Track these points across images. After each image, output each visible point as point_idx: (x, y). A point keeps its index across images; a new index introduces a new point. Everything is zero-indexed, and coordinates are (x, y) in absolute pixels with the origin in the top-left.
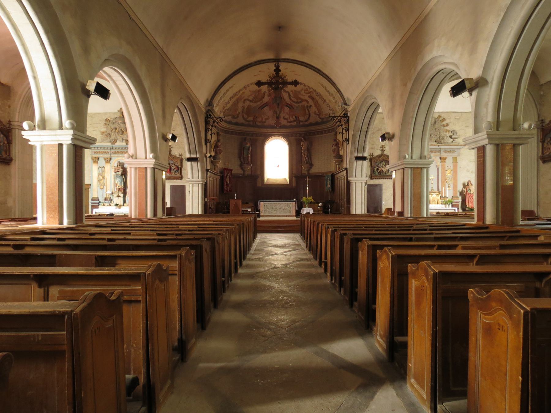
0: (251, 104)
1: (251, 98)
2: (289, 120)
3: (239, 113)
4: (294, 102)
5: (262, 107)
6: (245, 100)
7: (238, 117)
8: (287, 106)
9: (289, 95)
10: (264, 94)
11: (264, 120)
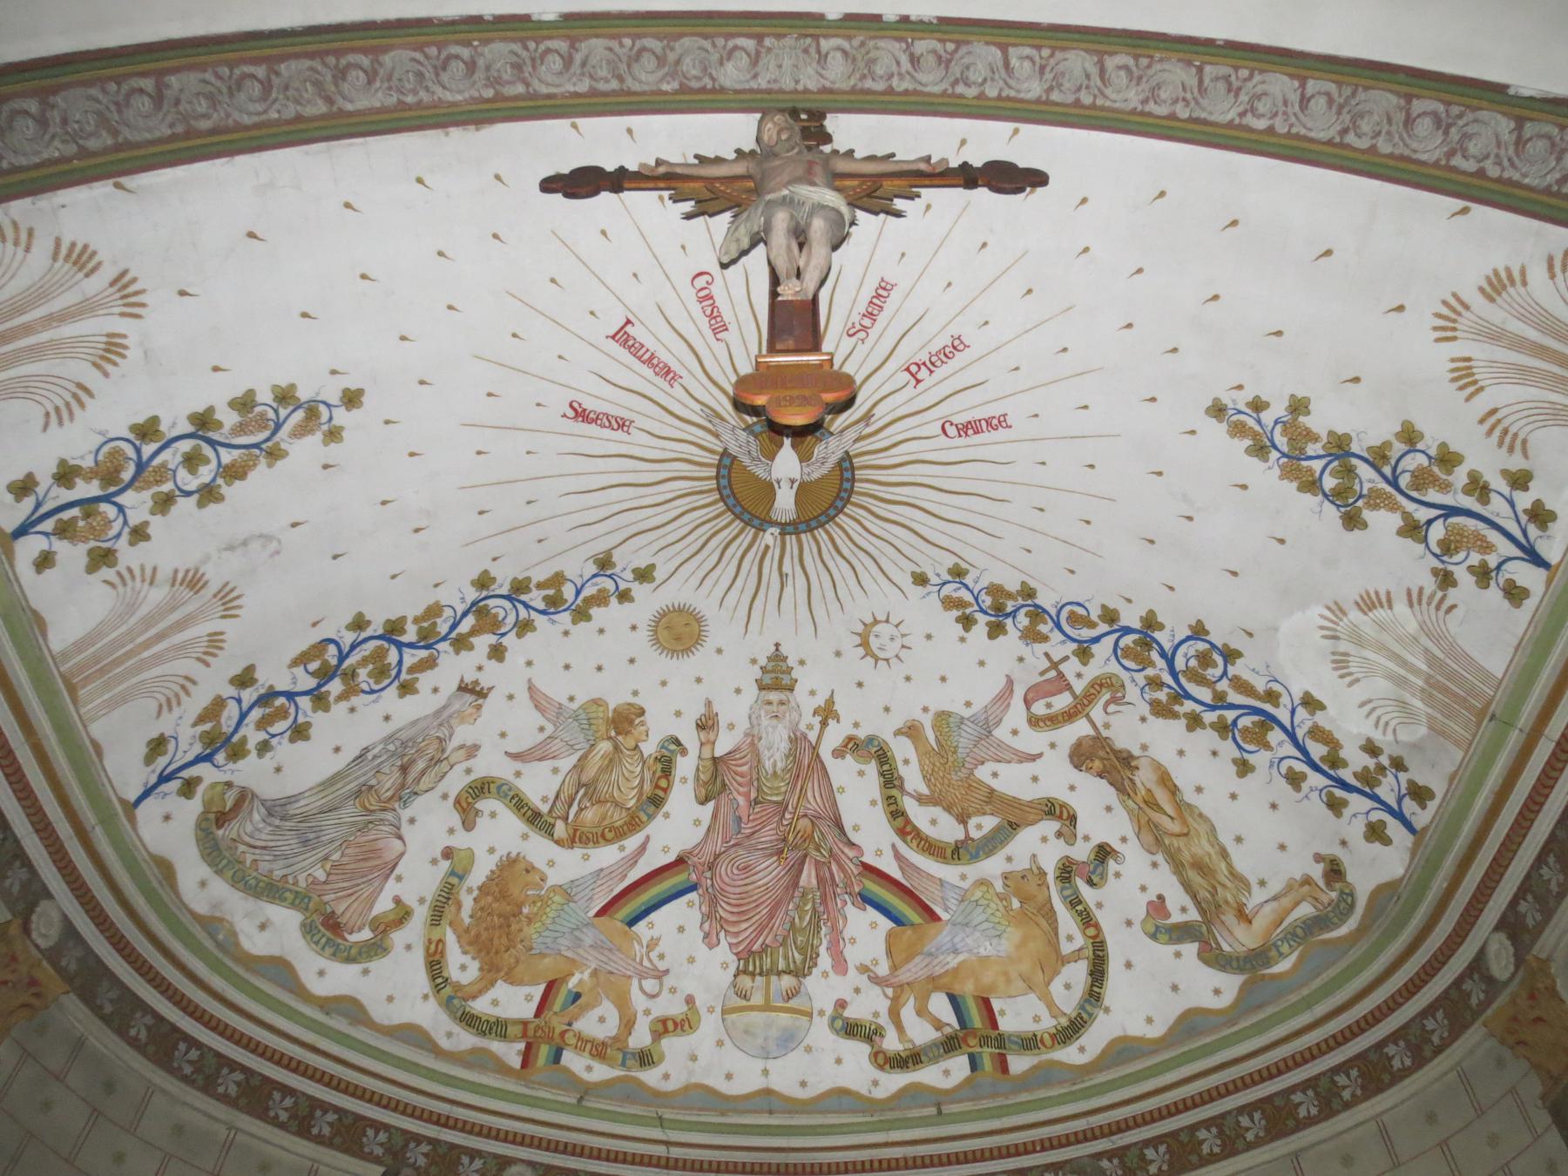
0: (538, 850)
1: (539, 785)
2: (892, 1043)
3: (402, 915)
4: (931, 848)
5: (634, 901)
6: (481, 788)
7: (376, 948)
8: (867, 900)
9: (890, 780)
10: (665, 765)
11: (640, 1038)
